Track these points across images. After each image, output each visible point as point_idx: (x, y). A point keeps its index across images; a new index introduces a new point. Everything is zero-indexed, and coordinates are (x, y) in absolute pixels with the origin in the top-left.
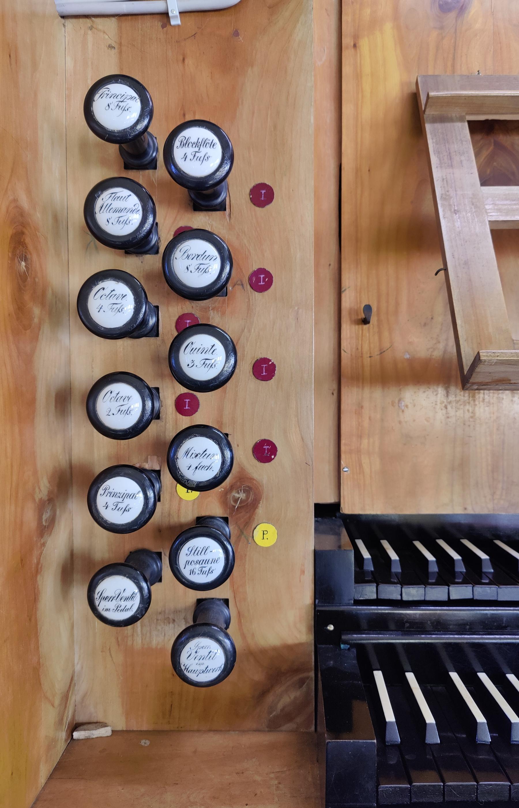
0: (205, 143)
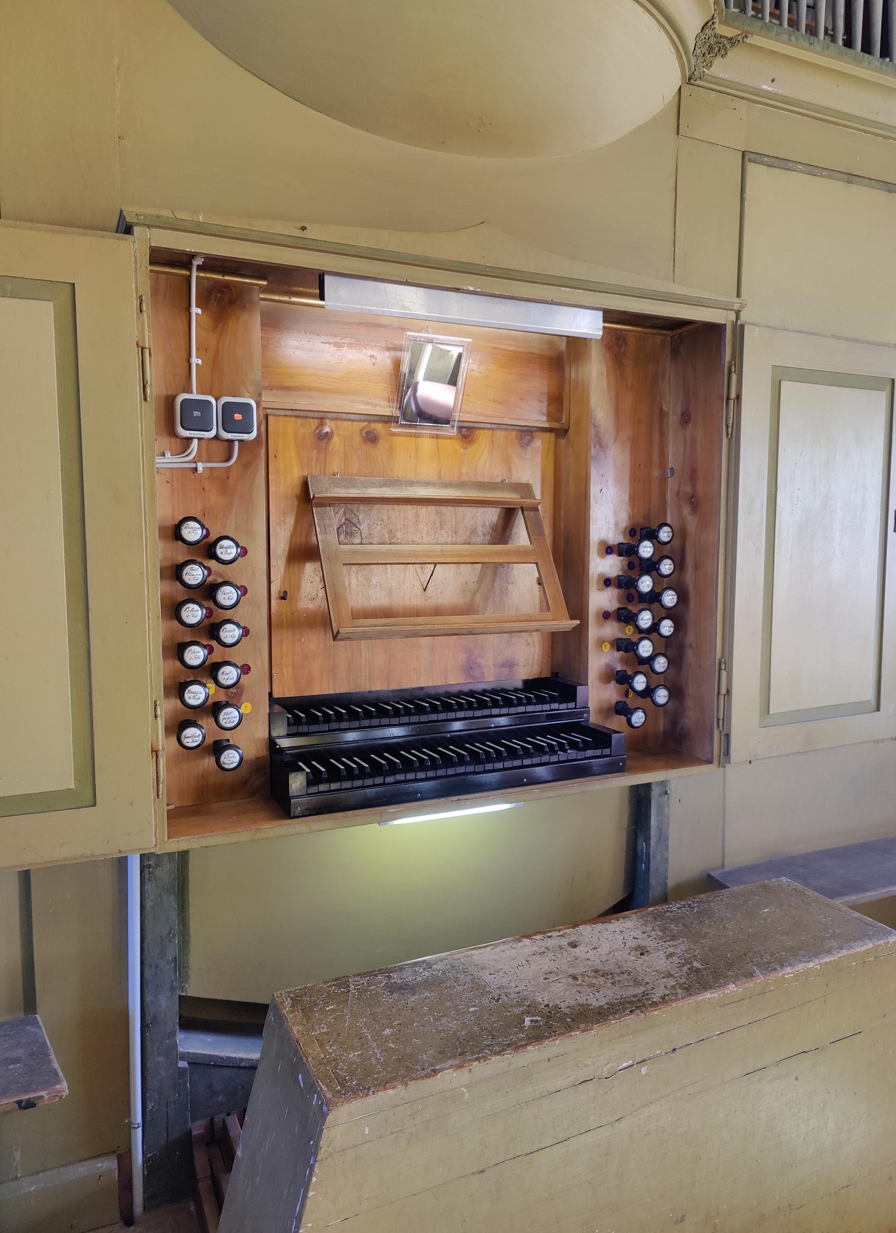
0: (230, 547)
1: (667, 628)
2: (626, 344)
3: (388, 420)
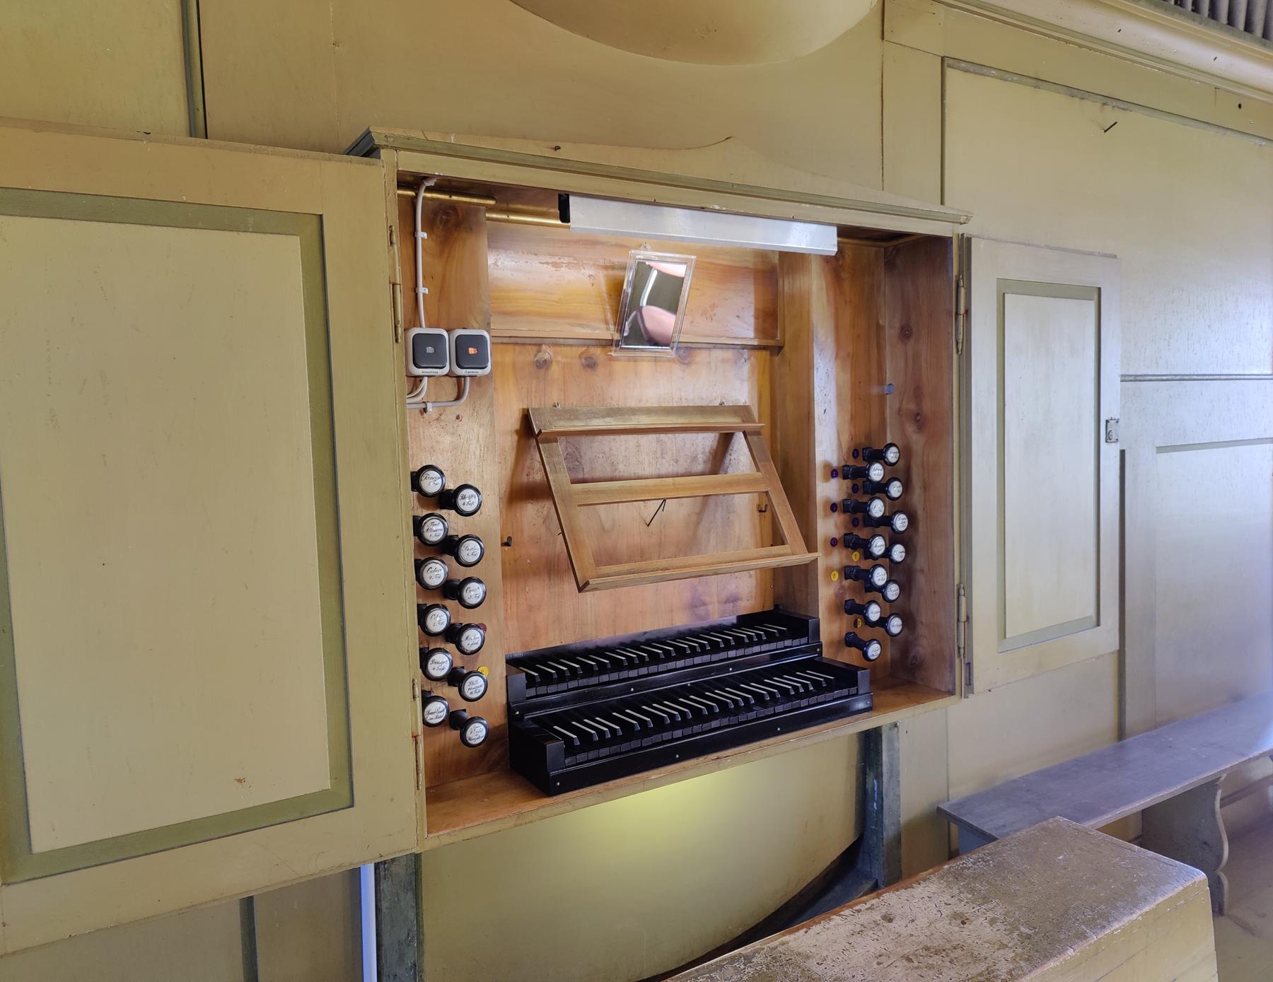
1: (898, 553)
3: (608, 344)
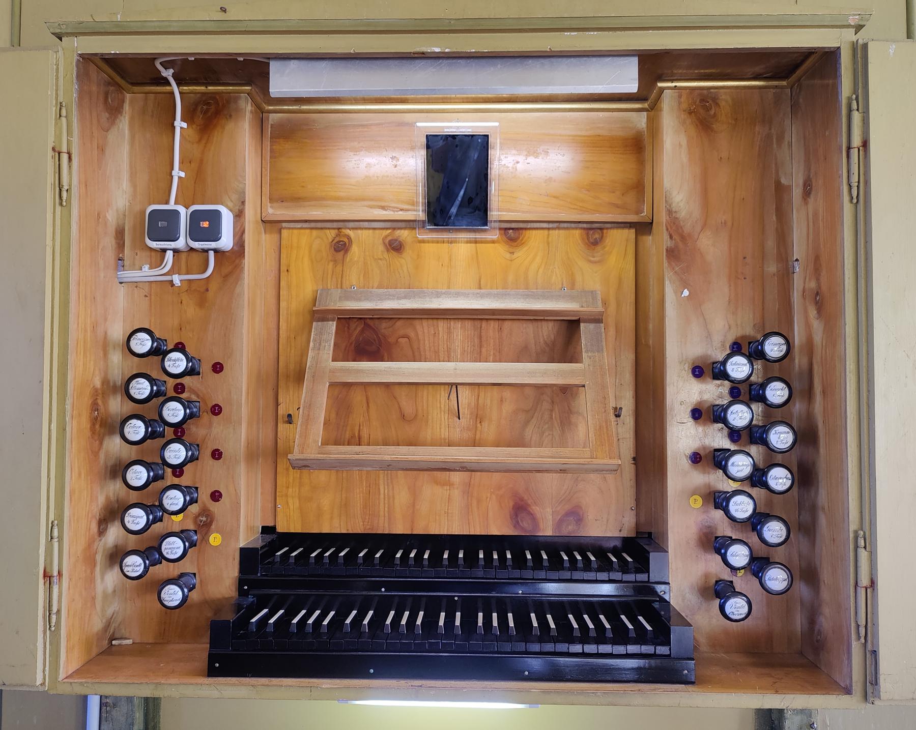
0: (178, 360)
2: (717, 104)
